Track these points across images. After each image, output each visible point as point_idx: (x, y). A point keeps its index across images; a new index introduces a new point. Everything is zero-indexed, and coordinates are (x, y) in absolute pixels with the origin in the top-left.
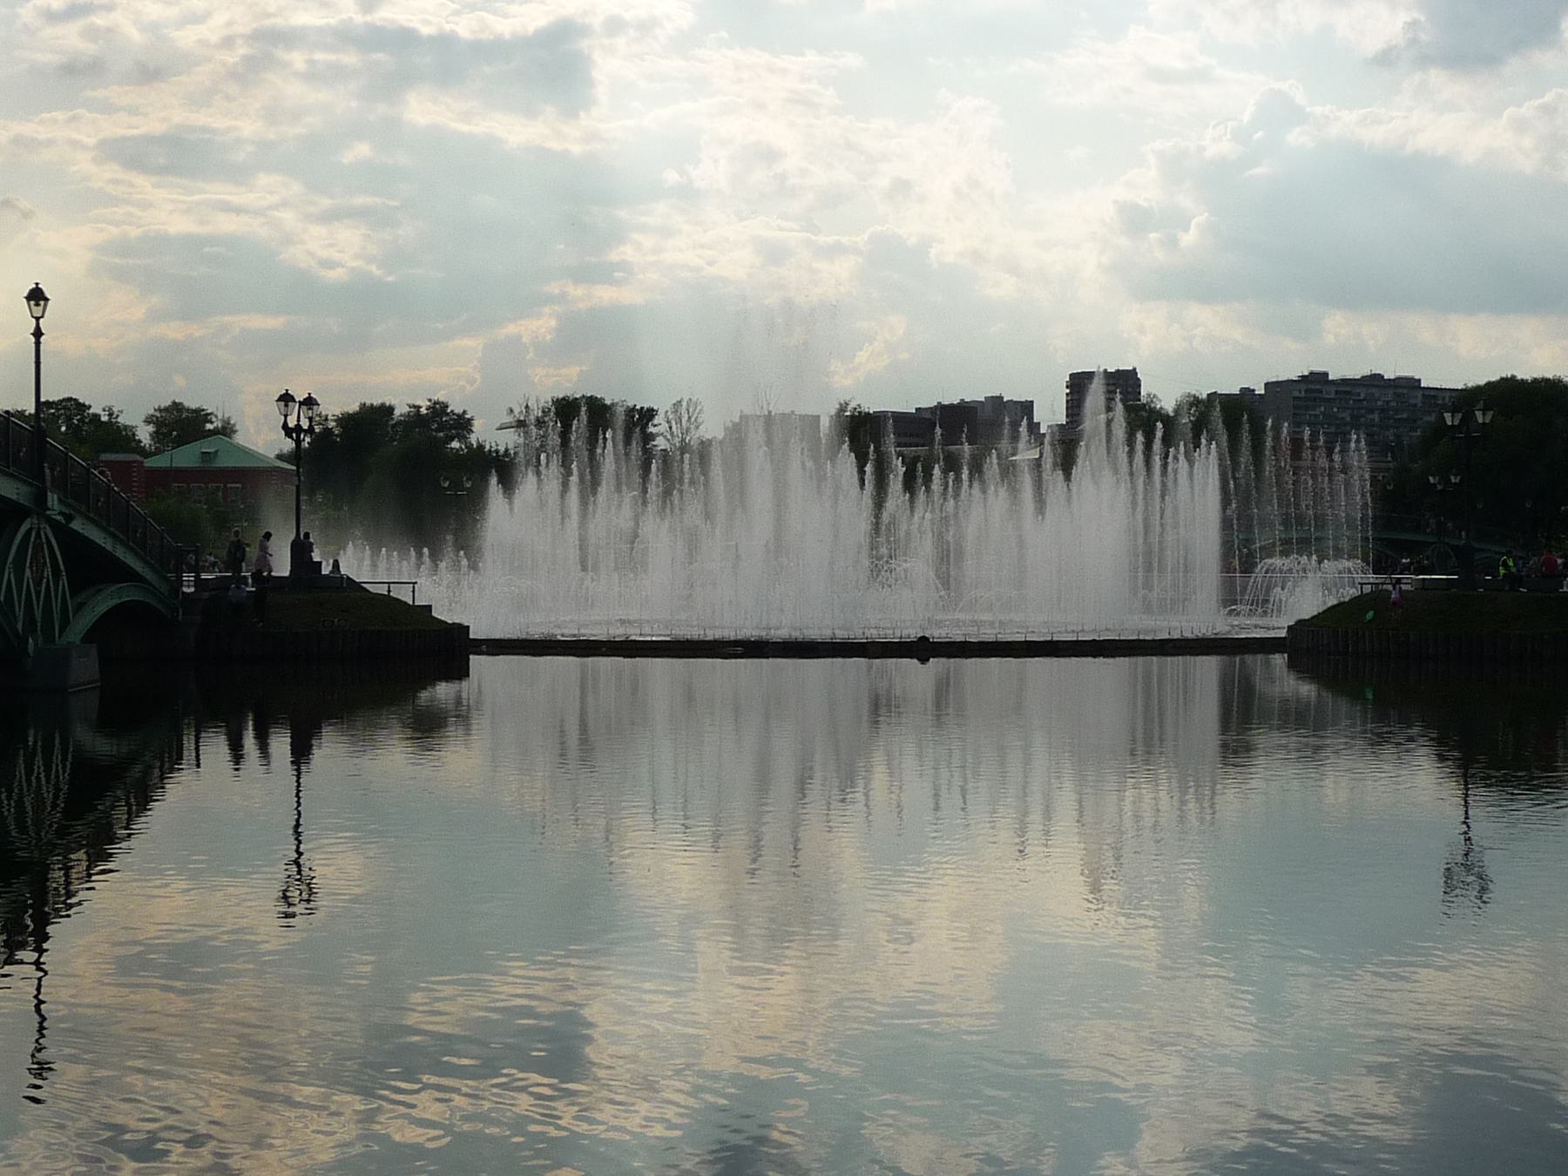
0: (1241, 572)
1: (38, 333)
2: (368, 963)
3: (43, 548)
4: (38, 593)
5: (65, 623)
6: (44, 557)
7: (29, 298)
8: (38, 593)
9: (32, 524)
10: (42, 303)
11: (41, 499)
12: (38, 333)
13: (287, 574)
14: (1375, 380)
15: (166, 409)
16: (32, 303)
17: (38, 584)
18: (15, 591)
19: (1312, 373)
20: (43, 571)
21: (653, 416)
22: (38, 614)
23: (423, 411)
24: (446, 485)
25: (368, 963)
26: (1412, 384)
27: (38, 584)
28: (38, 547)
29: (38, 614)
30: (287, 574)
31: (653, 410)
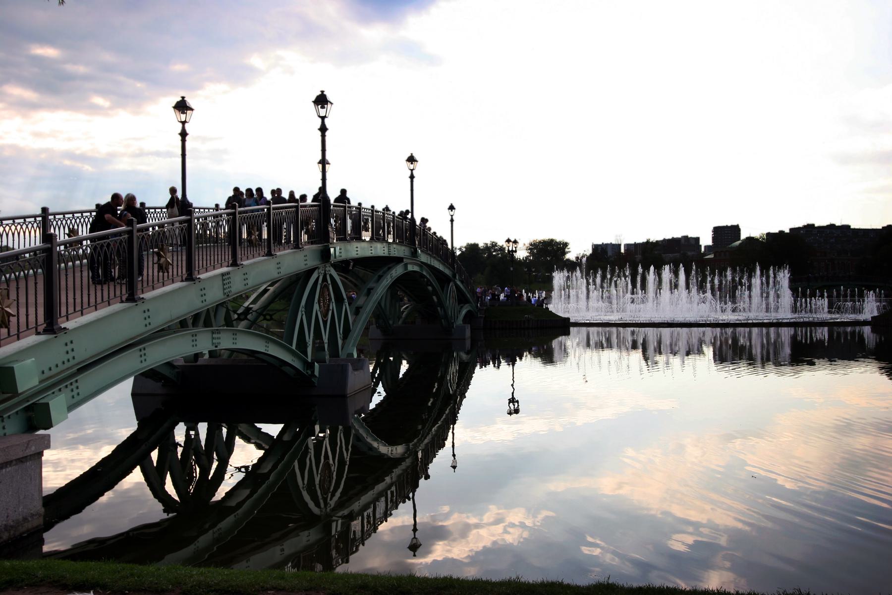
0: (885, 297)
1: (184, 134)
2: (628, 457)
3: (328, 290)
4: (325, 323)
5: (457, 317)
6: (329, 295)
7: (449, 209)
8: (325, 323)
9: (319, 273)
10: (453, 210)
11: (454, 276)
12: (184, 134)
13: (385, 394)
14: (832, 227)
15: (442, 239)
16: (450, 210)
17: (325, 315)
18: (433, 283)
19: (808, 225)
20: (329, 306)
21: (567, 246)
22: (325, 339)
23: (489, 245)
24: (534, 270)
25: (628, 457)
26: (847, 227)
27: (325, 315)
28: (325, 287)
29: (453, 316)
30: (385, 394)
31: (567, 243)
